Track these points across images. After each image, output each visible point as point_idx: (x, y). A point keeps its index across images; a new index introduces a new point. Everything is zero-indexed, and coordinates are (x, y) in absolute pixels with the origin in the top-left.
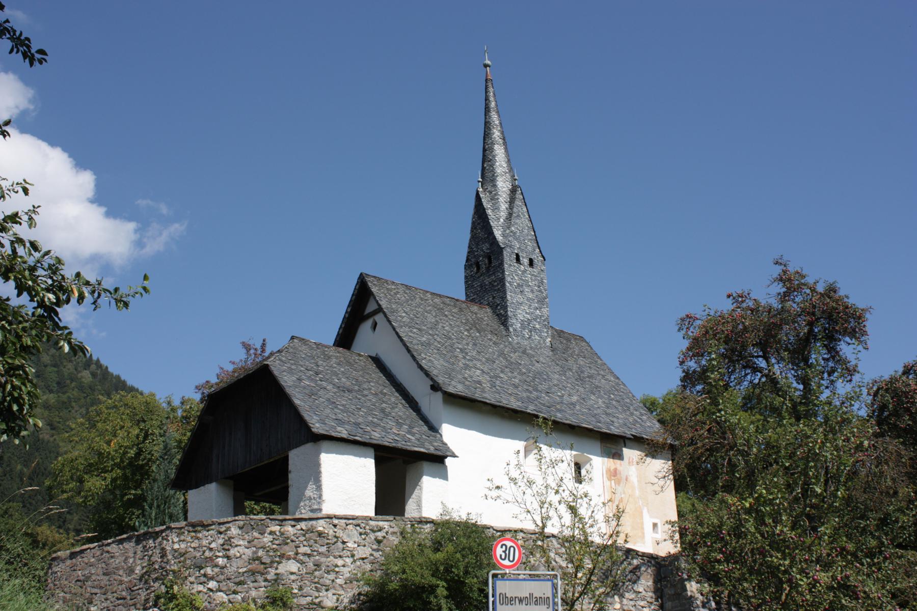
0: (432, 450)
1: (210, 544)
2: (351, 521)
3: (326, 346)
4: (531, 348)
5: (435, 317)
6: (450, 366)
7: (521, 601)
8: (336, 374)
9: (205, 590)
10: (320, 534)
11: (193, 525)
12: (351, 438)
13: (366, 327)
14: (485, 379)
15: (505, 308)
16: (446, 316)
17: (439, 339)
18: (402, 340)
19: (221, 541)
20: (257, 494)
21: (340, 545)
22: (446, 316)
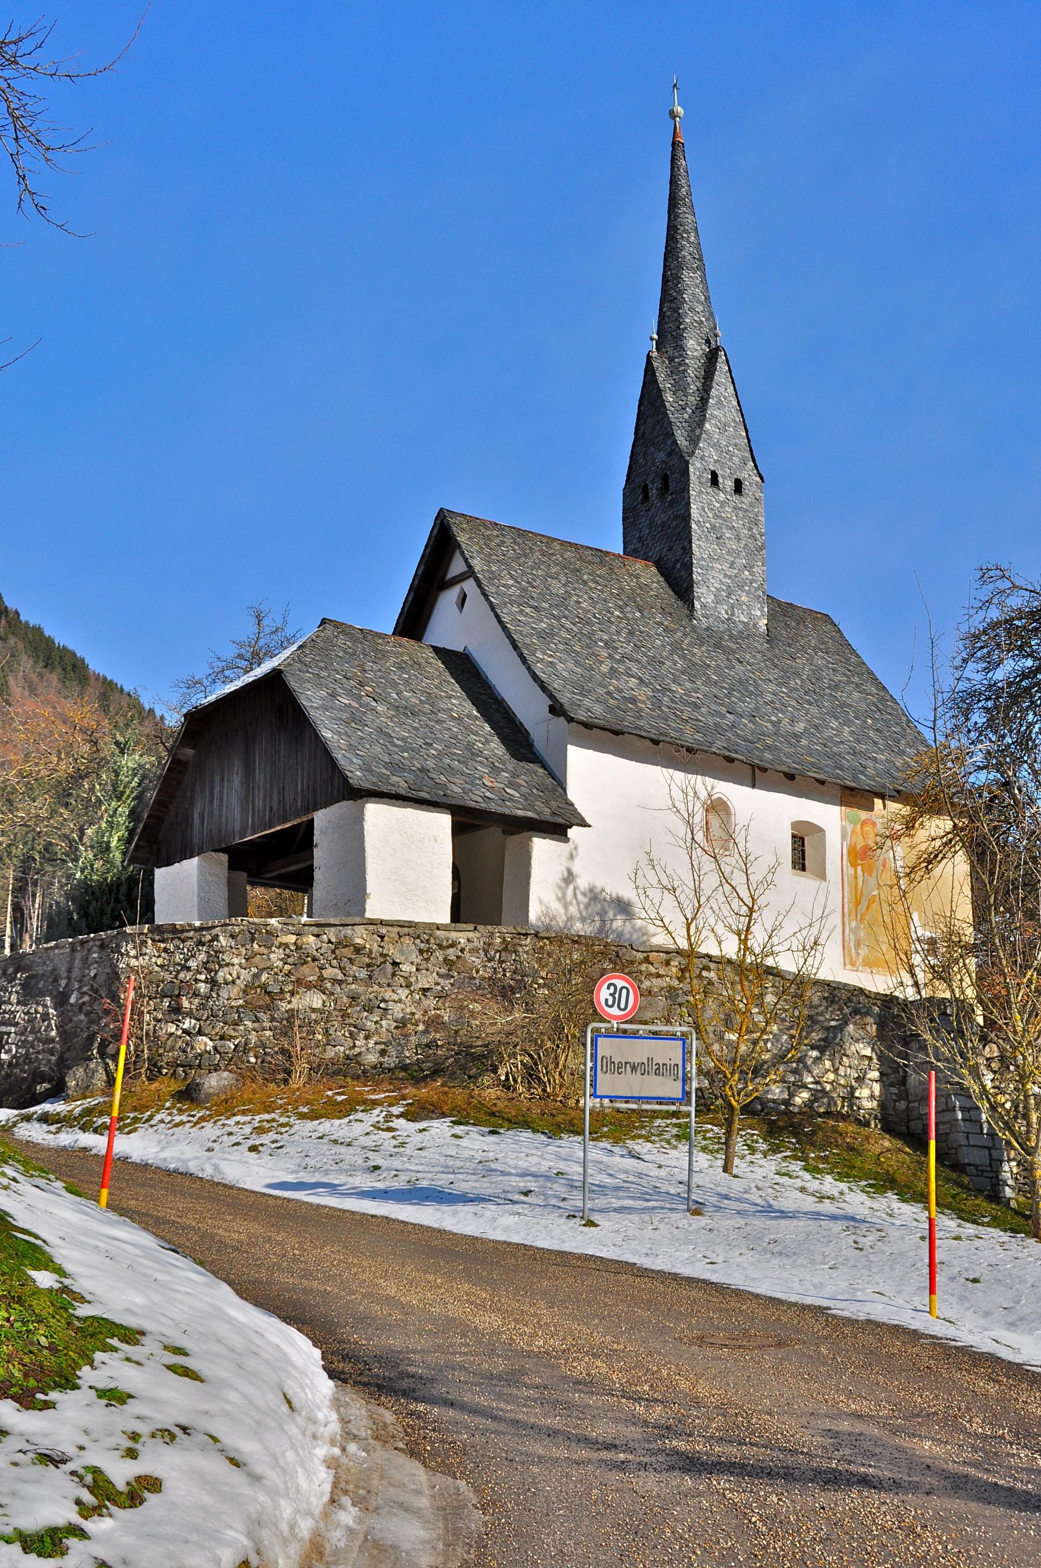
0: (546, 814)
1: (186, 960)
2: (406, 930)
3: (380, 635)
4: (731, 636)
5: (565, 585)
6: (587, 674)
7: (634, 1068)
8: (394, 685)
9: (180, 1032)
10: (358, 950)
11: (160, 930)
12: (414, 794)
13: (448, 599)
14: (643, 694)
15: (689, 567)
16: (585, 583)
17: (568, 625)
18: (505, 628)
19: (202, 957)
20: (268, 875)
21: (389, 969)
22: (585, 583)
